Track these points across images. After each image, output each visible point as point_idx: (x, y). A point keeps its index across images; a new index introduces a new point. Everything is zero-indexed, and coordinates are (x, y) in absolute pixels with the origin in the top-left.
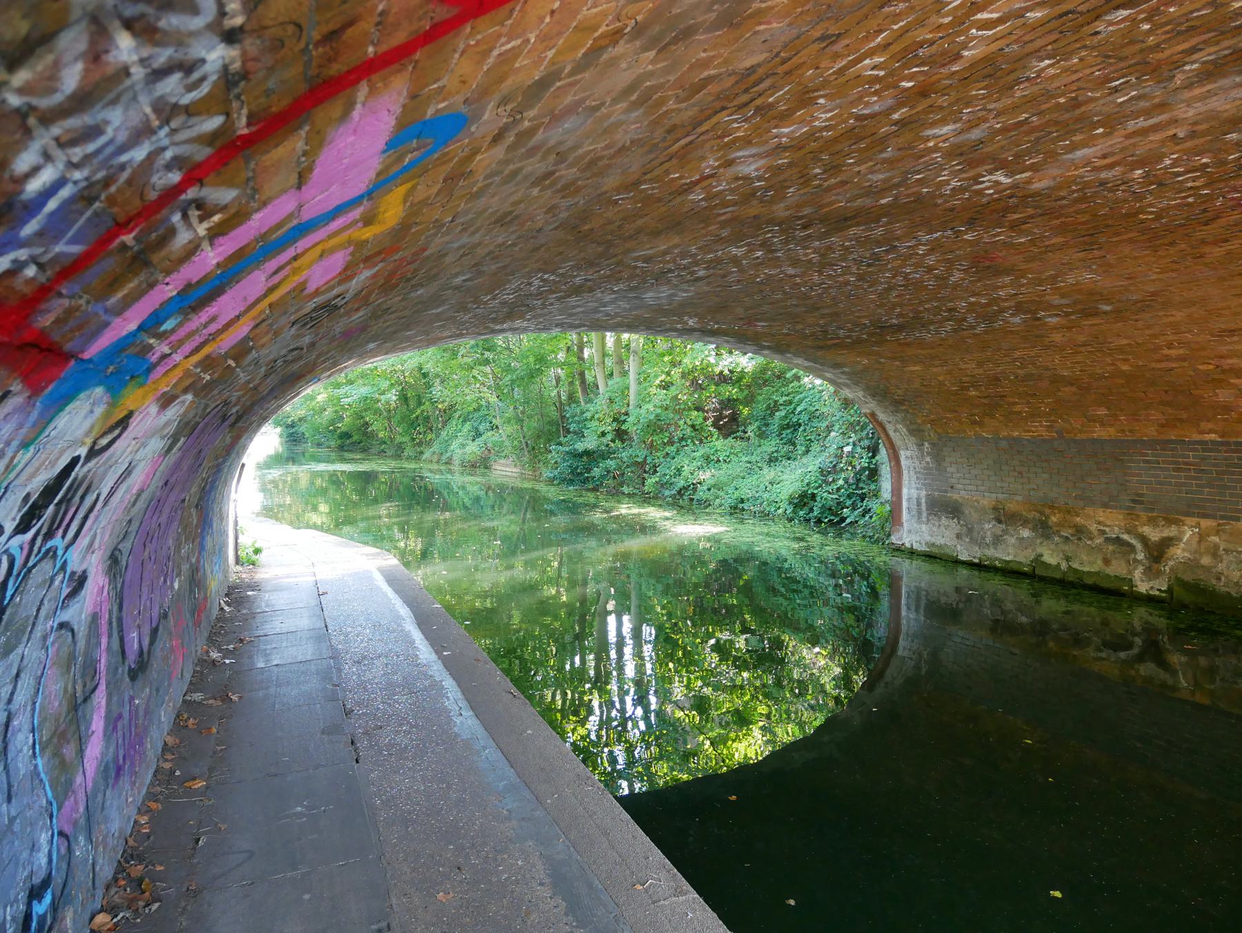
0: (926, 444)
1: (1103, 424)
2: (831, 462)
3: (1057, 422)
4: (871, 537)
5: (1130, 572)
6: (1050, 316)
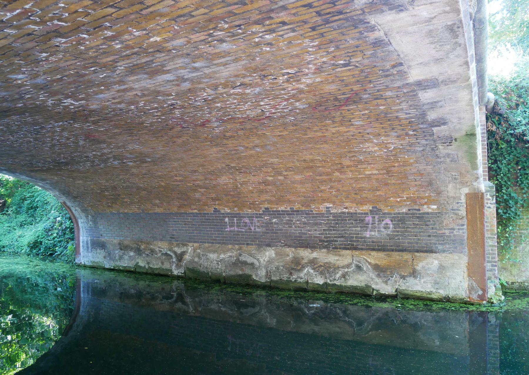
0: (90, 216)
1: (158, 207)
2: (50, 225)
3: (141, 206)
4: (67, 261)
5: (171, 267)
6: (129, 162)
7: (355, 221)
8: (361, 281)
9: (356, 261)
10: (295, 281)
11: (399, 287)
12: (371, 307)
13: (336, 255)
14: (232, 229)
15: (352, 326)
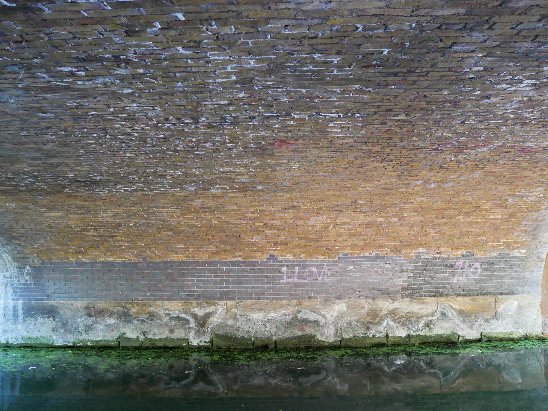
5: (187, 335)
7: (444, 266)
8: (447, 329)
9: (441, 308)
10: (373, 336)
11: (484, 331)
12: (458, 354)
13: (420, 303)
14: (290, 280)
15: (438, 378)
